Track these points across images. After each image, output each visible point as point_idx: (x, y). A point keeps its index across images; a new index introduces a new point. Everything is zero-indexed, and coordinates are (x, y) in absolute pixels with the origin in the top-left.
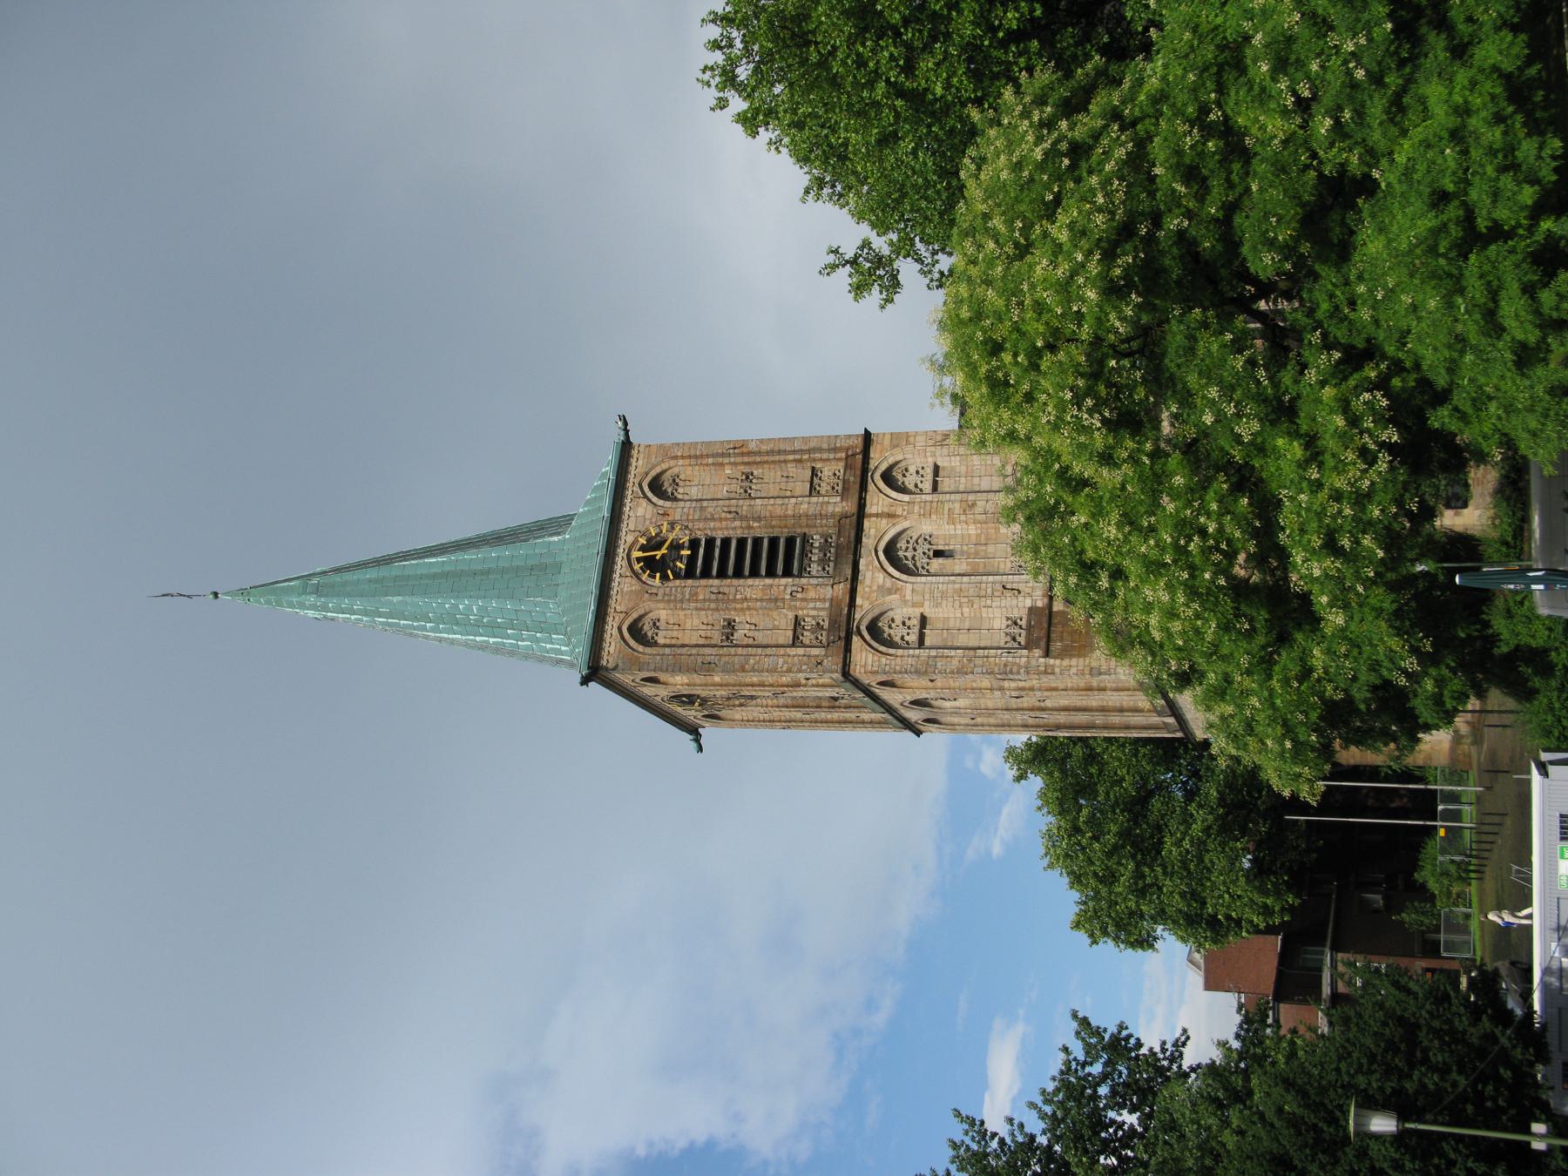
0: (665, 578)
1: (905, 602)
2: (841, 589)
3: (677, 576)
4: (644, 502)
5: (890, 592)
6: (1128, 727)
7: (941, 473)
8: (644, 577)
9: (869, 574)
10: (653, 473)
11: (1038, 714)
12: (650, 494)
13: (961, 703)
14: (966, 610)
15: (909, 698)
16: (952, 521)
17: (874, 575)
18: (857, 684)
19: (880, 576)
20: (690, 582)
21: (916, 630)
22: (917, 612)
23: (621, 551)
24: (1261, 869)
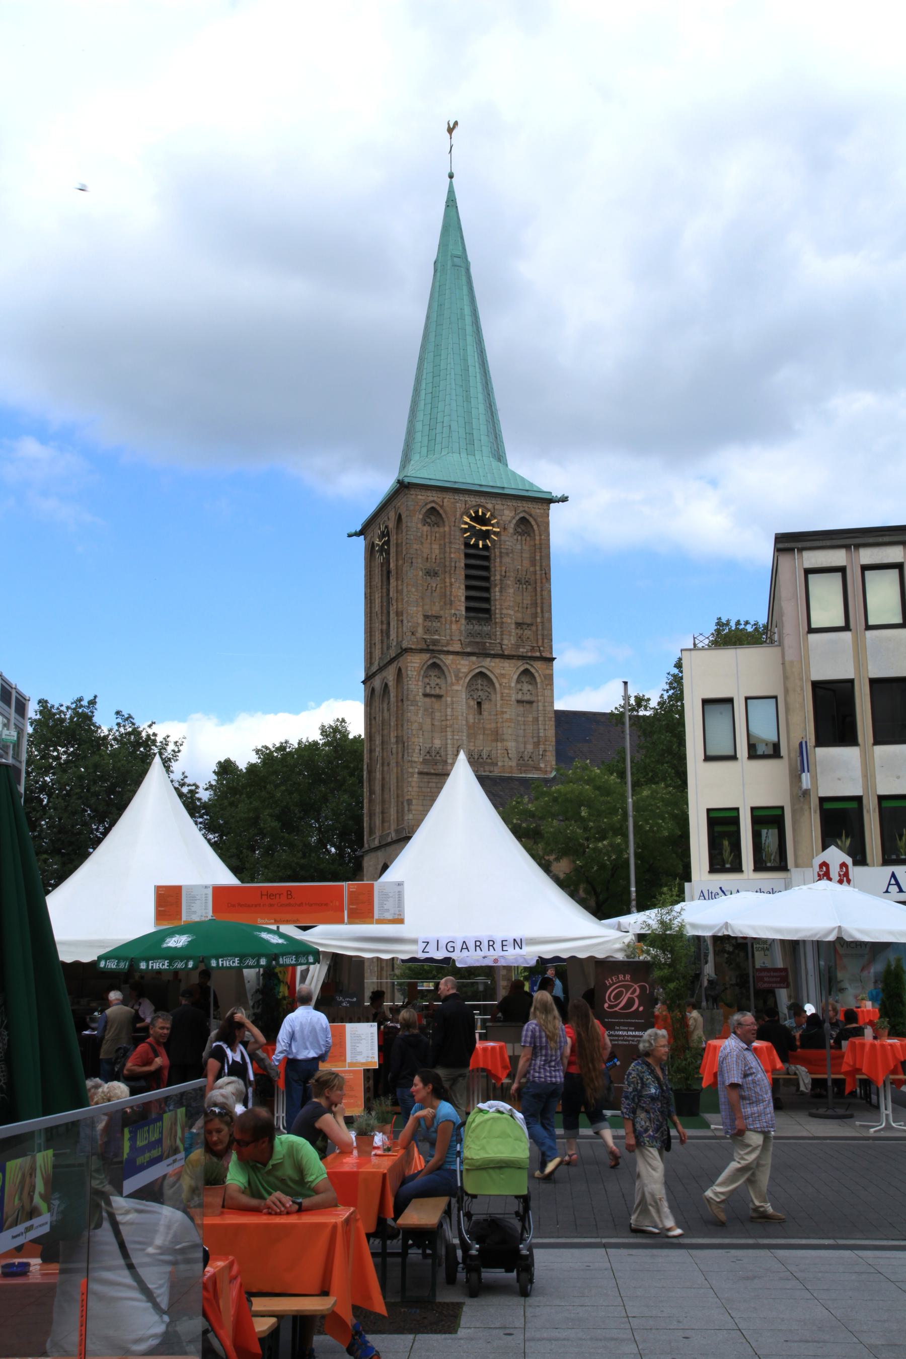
2: (457, 647)
4: (512, 514)
6: (371, 815)
7: (528, 706)
9: (466, 663)
10: (531, 520)
21: (433, 692)
23: (482, 500)
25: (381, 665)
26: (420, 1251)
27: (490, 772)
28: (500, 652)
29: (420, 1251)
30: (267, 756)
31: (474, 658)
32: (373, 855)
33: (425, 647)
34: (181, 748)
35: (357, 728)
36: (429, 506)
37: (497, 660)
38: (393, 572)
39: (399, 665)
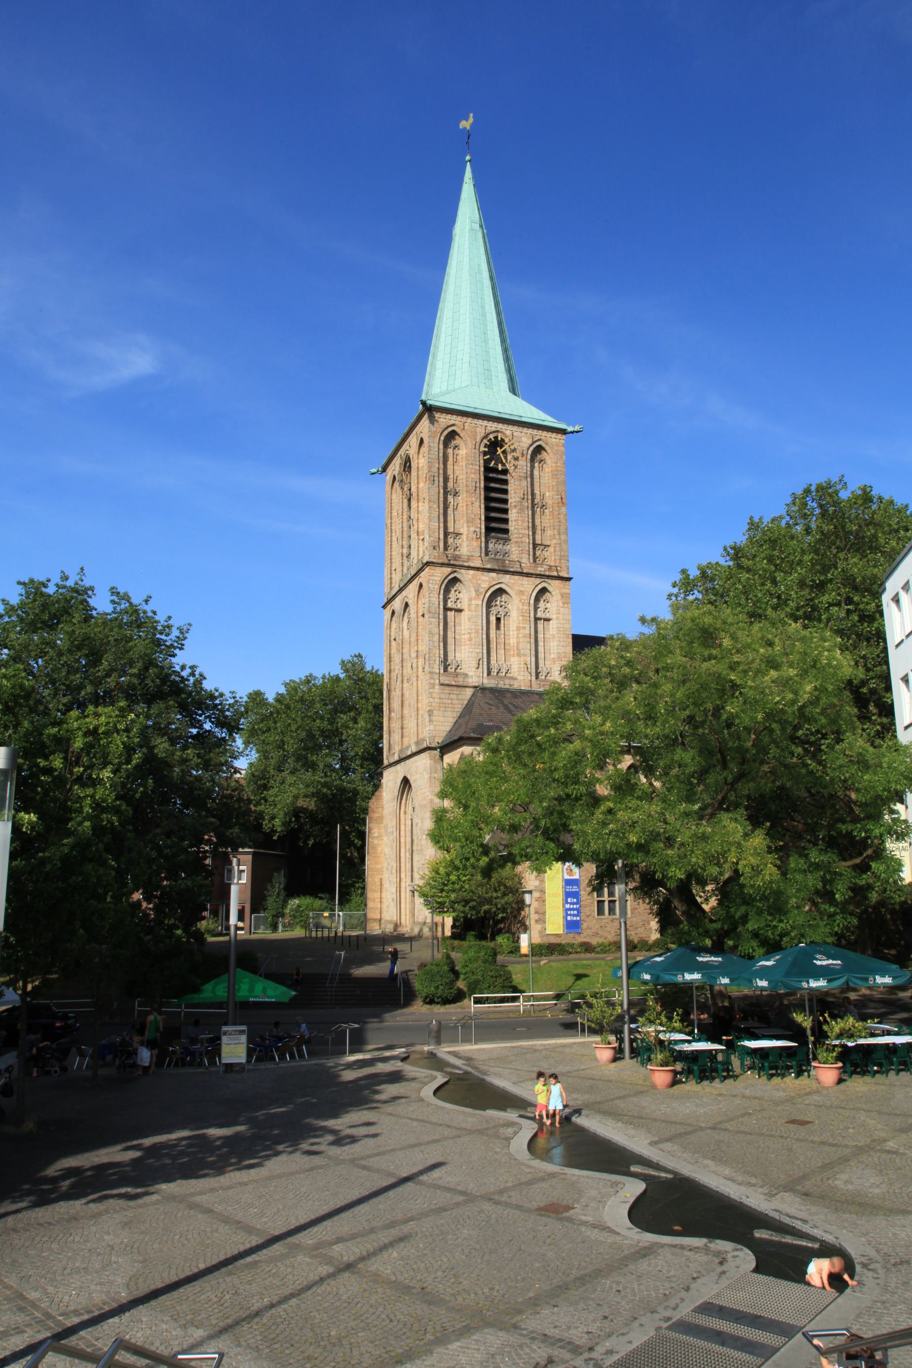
0: (485, 453)
1: (470, 600)
2: (478, 563)
4: (530, 442)
5: (477, 591)
8: (485, 441)
9: (487, 578)
12: (534, 446)
15: (410, 602)
16: (518, 628)
17: (487, 581)
18: (421, 570)
21: (454, 607)
22: (553, 617)
24: (297, 812)
28: (519, 570)
30: (292, 687)
31: (494, 575)
33: (446, 561)
34: (187, 635)
37: (516, 577)
38: (415, 495)
39: (421, 580)
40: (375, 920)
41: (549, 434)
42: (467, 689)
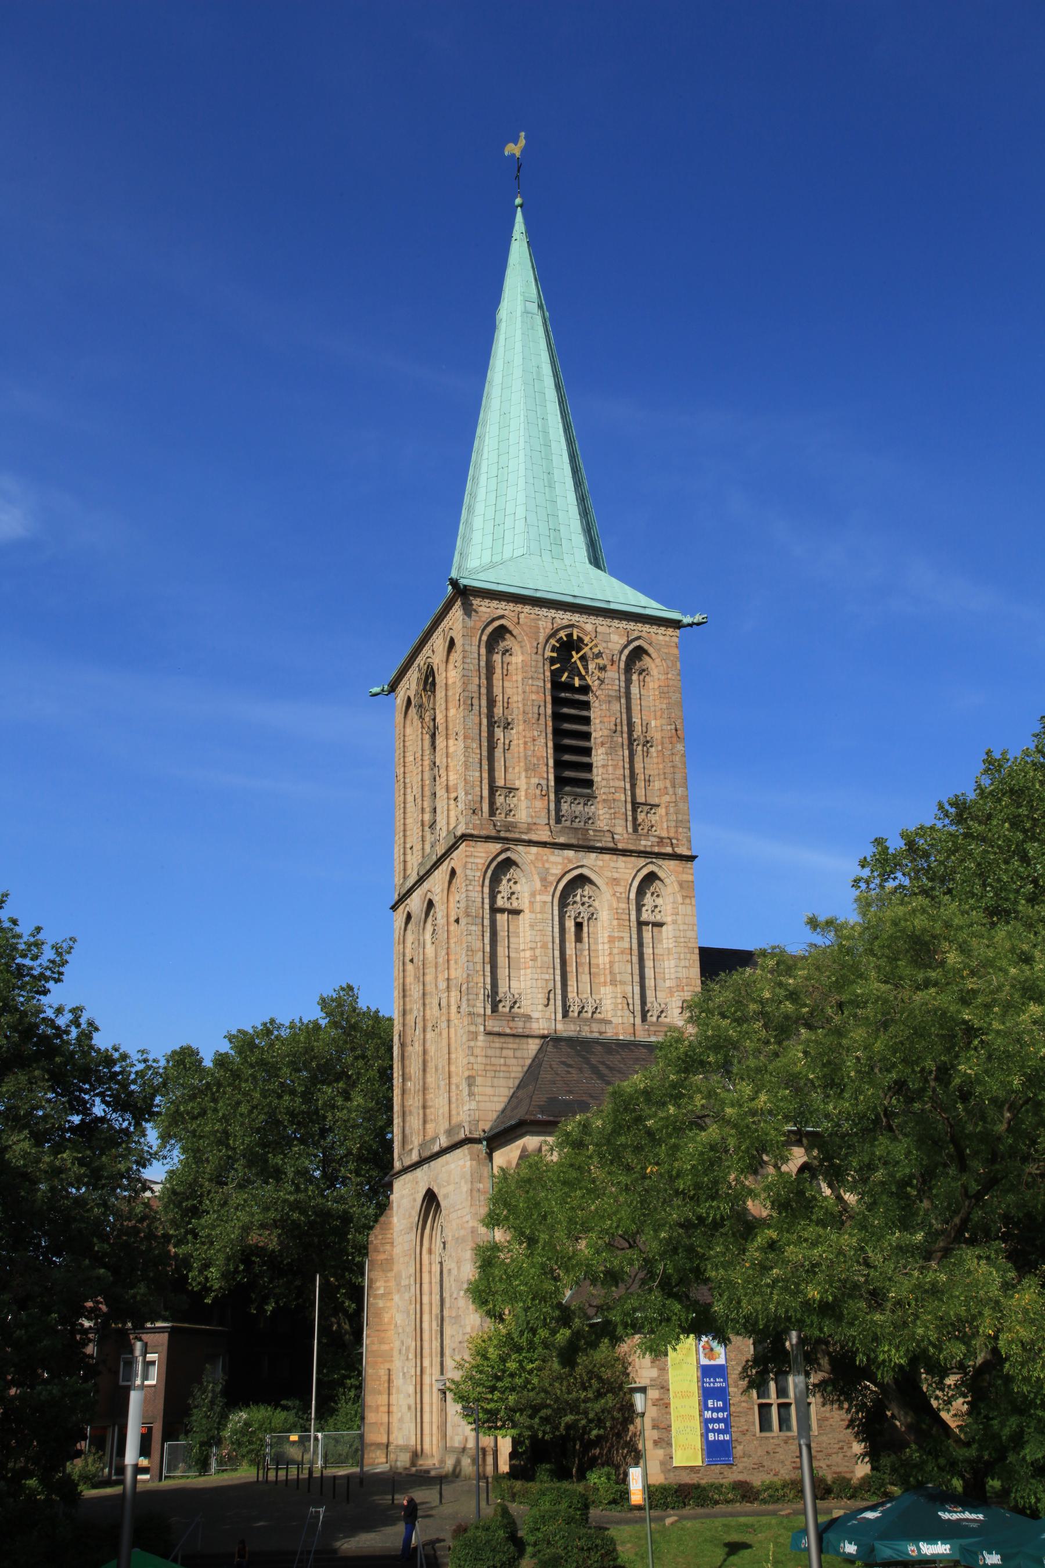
0: (553, 661)
1: (533, 894)
2: (544, 836)
3: (553, 673)
5: (543, 880)
7: (656, 929)
9: (559, 859)
10: (651, 650)
11: (420, 1026)
13: (430, 950)
14: (528, 954)
15: (436, 899)
17: (558, 863)
19: (557, 871)
20: (549, 685)
21: (507, 906)
23: (576, 618)
25: (421, 874)
26: (365, 1469)
27: (601, 1033)
28: (611, 845)
29: (365, 1469)
30: (244, 1043)
31: (570, 853)
32: (408, 1177)
33: (493, 833)
34: (67, 957)
35: (518, 155)
36: (496, 624)
37: (607, 857)
38: (441, 728)
39: (453, 864)
40: (378, 1445)
41: (654, 629)
42: (530, 1041)
